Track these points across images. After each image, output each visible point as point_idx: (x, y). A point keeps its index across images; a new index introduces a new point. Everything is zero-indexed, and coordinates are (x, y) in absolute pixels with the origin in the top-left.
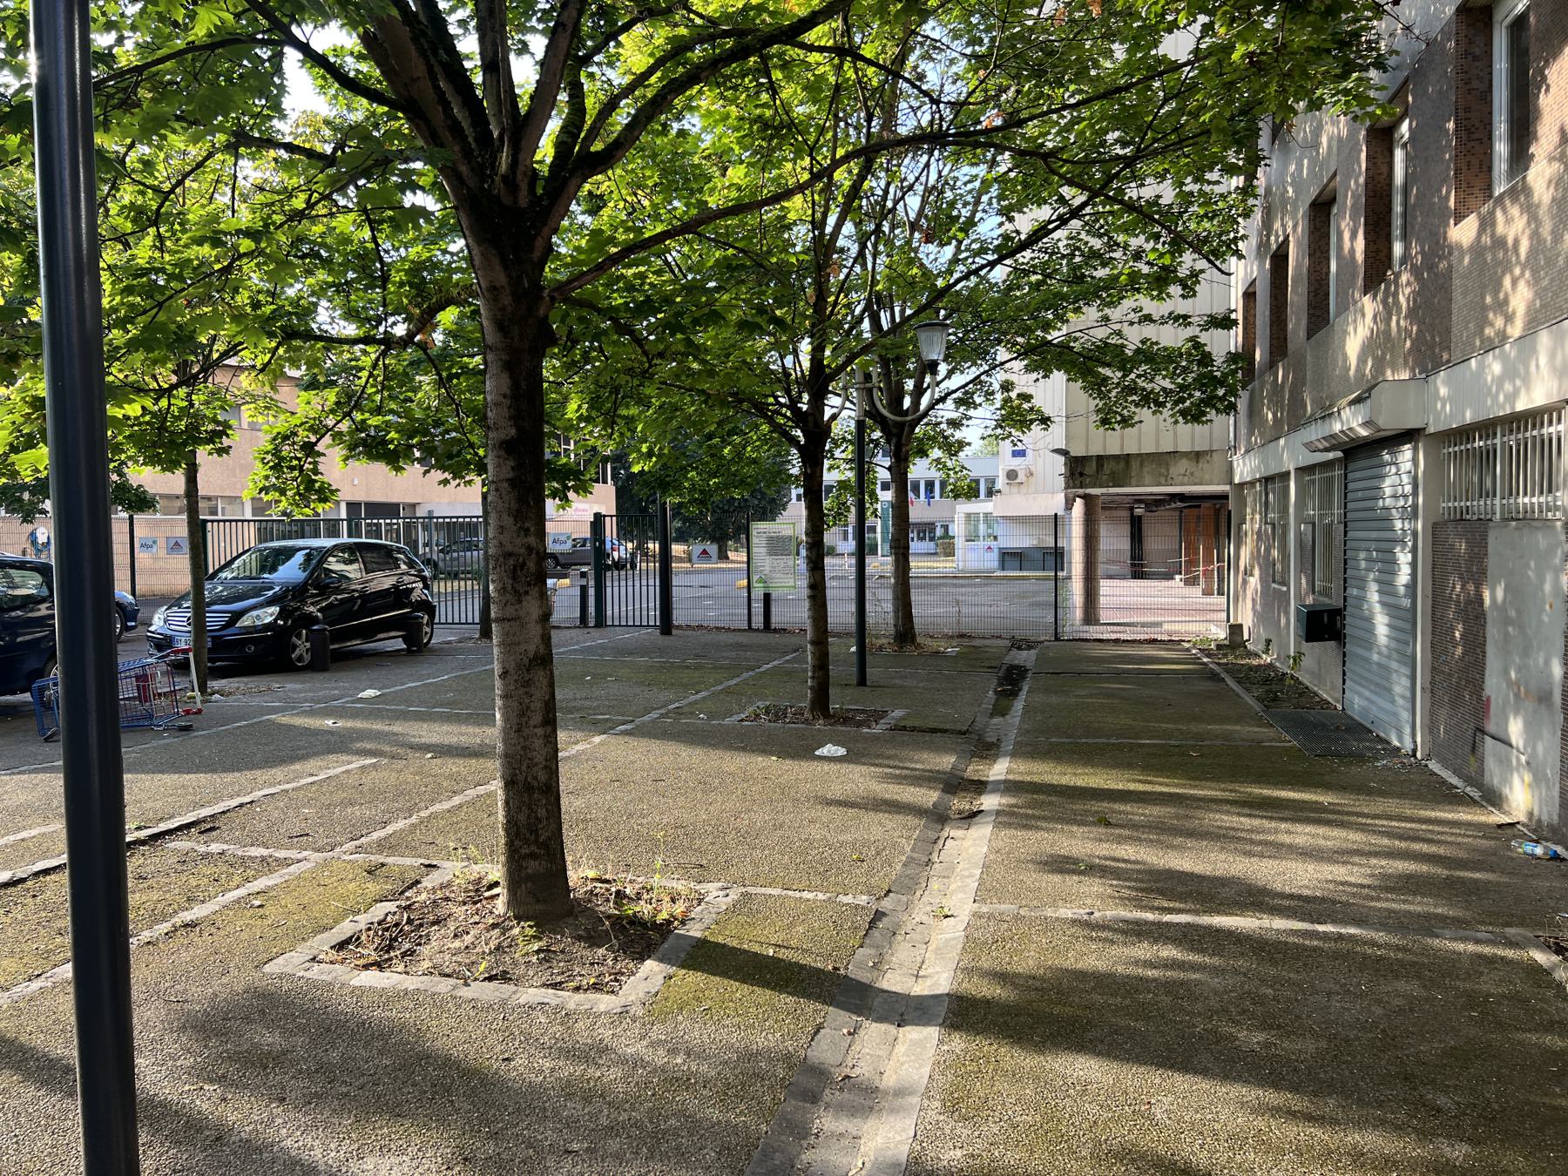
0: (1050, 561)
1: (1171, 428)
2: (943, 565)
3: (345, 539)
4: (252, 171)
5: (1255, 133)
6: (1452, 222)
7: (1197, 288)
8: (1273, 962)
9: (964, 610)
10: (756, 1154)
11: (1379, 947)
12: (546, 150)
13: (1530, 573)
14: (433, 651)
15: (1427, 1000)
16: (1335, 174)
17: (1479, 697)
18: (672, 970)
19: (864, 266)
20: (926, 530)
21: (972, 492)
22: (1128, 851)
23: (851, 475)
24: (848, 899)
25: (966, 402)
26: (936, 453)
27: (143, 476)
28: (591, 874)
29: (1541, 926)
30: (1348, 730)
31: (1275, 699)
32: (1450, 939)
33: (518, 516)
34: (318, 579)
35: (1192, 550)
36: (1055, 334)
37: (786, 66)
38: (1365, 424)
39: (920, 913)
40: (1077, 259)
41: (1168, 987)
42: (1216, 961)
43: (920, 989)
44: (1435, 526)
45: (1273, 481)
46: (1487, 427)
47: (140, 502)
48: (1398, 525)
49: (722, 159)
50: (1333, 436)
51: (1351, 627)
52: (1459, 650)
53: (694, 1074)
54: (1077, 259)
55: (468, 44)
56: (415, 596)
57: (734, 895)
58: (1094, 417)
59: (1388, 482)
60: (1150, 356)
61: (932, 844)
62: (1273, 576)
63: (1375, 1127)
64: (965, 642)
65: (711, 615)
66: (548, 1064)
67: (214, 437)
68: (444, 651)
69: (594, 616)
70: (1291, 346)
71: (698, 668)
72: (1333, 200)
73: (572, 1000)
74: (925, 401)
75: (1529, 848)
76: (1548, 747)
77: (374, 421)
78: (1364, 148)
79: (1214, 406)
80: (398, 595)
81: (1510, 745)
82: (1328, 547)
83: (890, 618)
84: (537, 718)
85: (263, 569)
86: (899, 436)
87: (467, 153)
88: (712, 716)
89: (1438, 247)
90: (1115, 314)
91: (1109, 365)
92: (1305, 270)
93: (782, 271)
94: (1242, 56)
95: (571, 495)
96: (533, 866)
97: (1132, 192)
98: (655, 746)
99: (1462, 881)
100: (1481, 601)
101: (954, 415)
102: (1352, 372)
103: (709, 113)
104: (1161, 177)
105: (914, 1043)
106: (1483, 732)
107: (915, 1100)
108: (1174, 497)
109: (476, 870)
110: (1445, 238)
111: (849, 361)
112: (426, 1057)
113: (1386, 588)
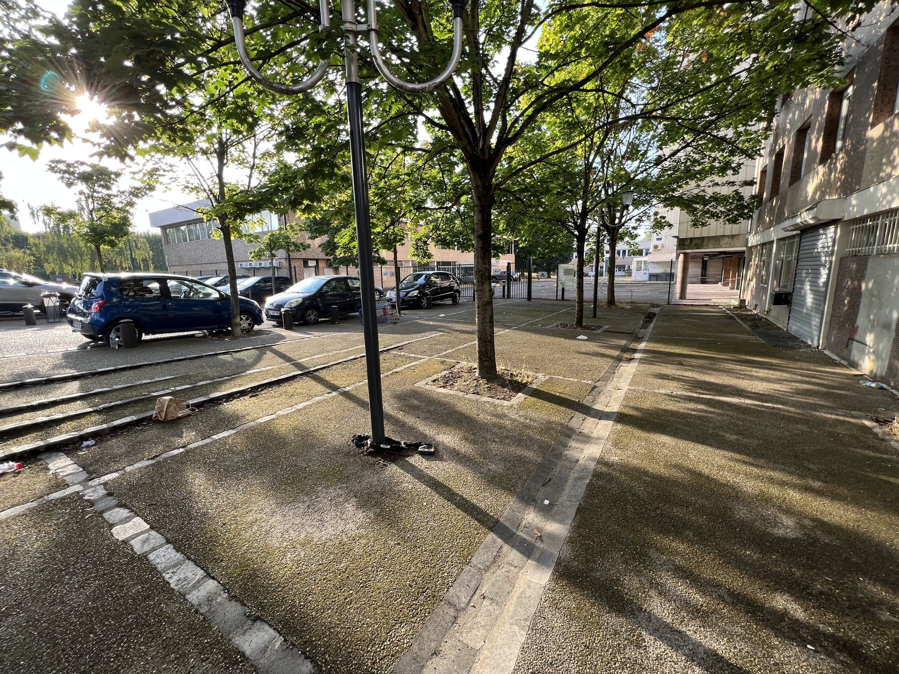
0: (668, 277)
1: (722, 226)
2: (628, 279)
3: (436, 271)
4: (409, 160)
5: (774, 103)
6: (869, 128)
7: (740, 170)
8: (744, 413)
9: (634, 294)
10: (550, 449)
11: (791, 413)
12: (494, 140)
13: (888, 276)
14: (460, 304)
15: (810, 432)
16: (811, 116)
17: (853, 326)
18: (527, 396)
19: (603, 172)
20: (622, 267)
21: (640, 253)
22: (689, 374)
23: (594, 247)
24: (585, 381)
25: (639, 220)
26: (627, 239)
27: (385, 254)
28: (503, 368)
29: (870, 412)
30: (788, 338)
31: (757, 326)
32: (824, 413)
33: (483, 259)
34: (429, 283)
35: (727, 273)
36: (676, 193)
37: (578, 101)
38: (813, 218)
39: (609, 387)
40: (688, 163)
41: (699, 417)
42: (720, 411)
43: (607, 410)
44: (841, 259)
45: (766, 245)
46: (874, 216)
47: (383, 262)
48: (823, 259)
49: (553, 139)
50: (797, 224)
51: (795, 299)
52: (846, 308)
53: (531, 425)
54: (688, 163)
55: (471, 110)
56: (455, 288)
57: (547, 377)
58: (690, 223)
59: (821, 241)
60: (716, 198)
61: (614, 368)
62: (761, 281)
63: (780, 471)
64: (633, 305)
65: (544, 295)
66: (489, 418)
67: (401, 240)
68: (463, 304)
69: (507, 295)
70: (781, 190)
71: (539, 311)
72: (809, 127)
73: (497, 402)
74: (623, 220)
75: (868, 384)
76: (886, 346)
77: (443, 233)
78: (827, 102)
79: (742, 217)
80: (451, 288)
81: (866, 345)
82: (788, 269)
83: (606, 296)
84: (488, 321)
85: (414, 280)
86: (613, 233)
87: (469, 142)
88: (542, 325)
89: (860, 140)
90: (702, 184)
91: (698, 203)
92: (791, 158)
93: (572, 176)
94: (771, 68)
95: (500, 254)
96: (486, 364)
97: (715, 133)
98: (524, 333)
99: (833, 393)
100: (860, 288)
101: (635, 225)
102: (809, 199)
103: (550, 122)
104: (728, 127)
105: (604, 425)
106: (853, 340)
107: (603, 441)
108: (721, 253)
109: (470, 364)
110: (865, 136)
111: (596, 206)
112: (456, 412)
113: (814, 284)
